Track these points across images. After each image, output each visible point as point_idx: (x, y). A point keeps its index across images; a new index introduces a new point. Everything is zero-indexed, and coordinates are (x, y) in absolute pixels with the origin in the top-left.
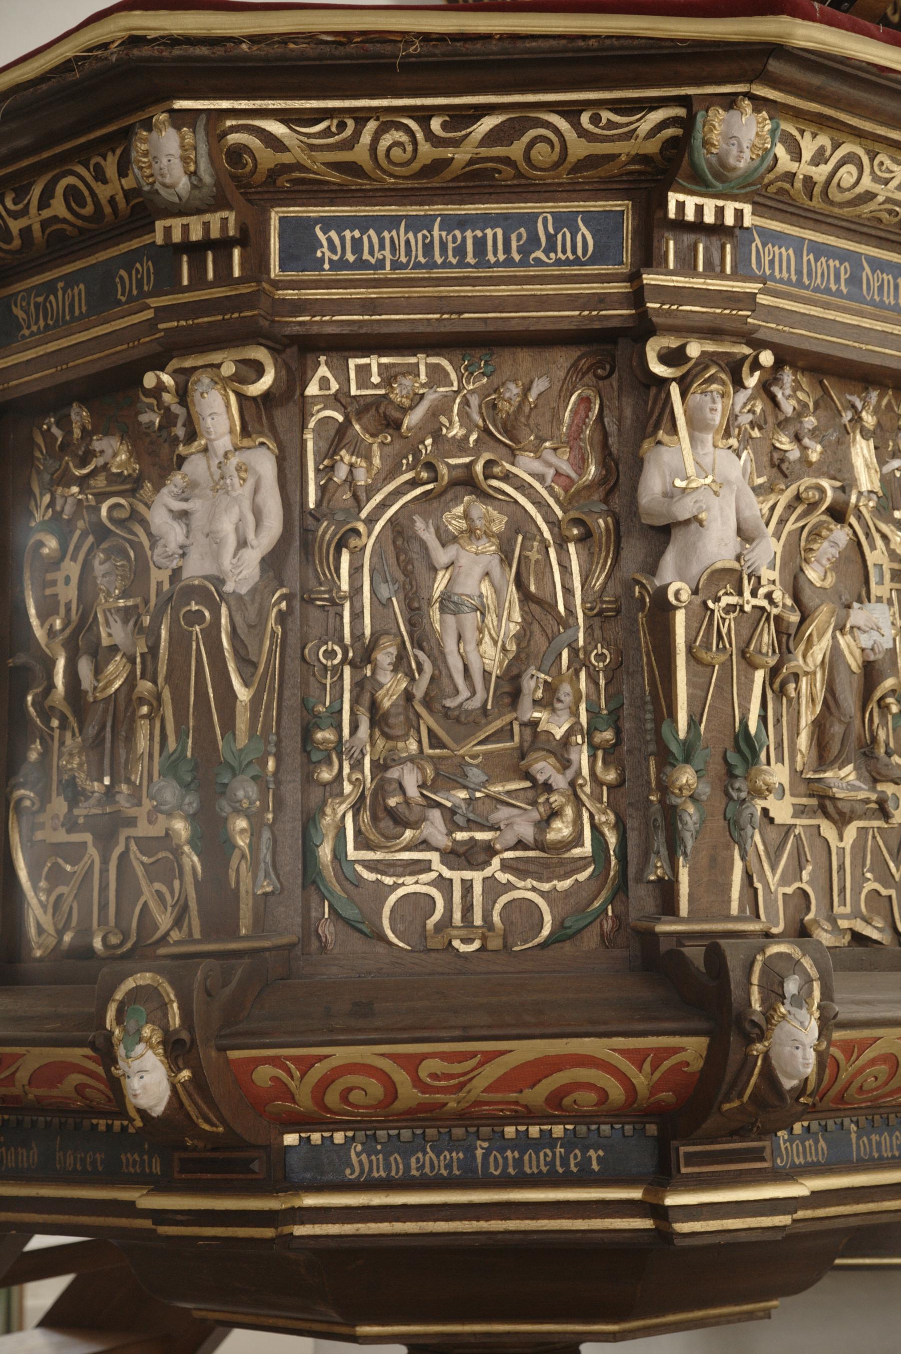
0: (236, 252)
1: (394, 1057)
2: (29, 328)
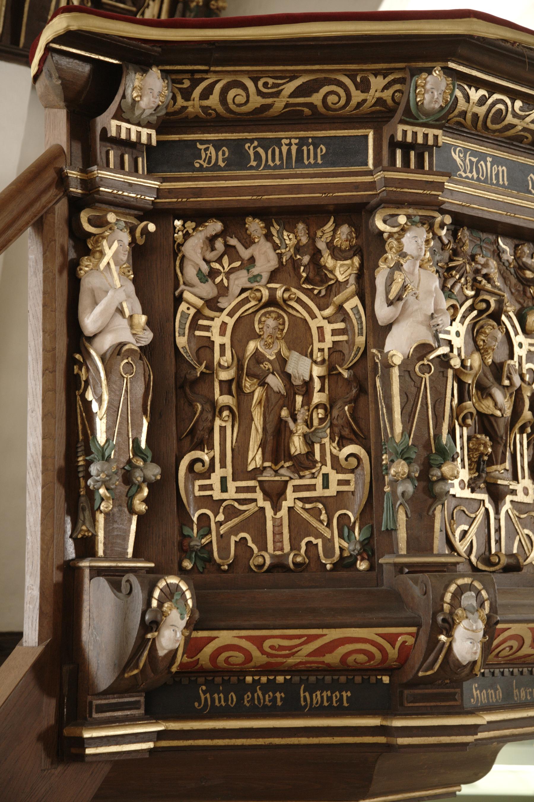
0: (412, 153)
1: (248, 638)
2: (465, 172)
